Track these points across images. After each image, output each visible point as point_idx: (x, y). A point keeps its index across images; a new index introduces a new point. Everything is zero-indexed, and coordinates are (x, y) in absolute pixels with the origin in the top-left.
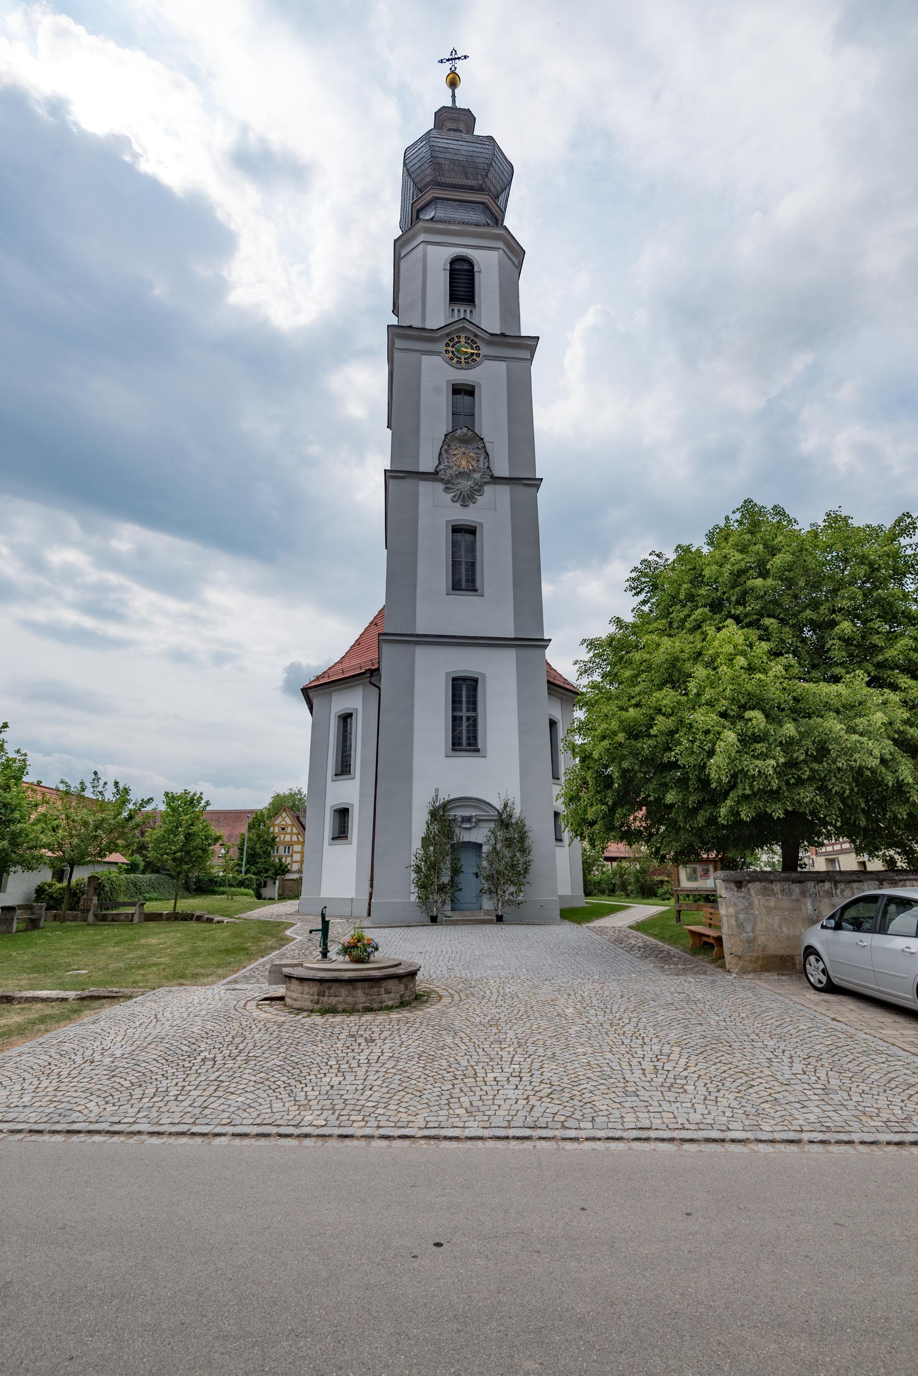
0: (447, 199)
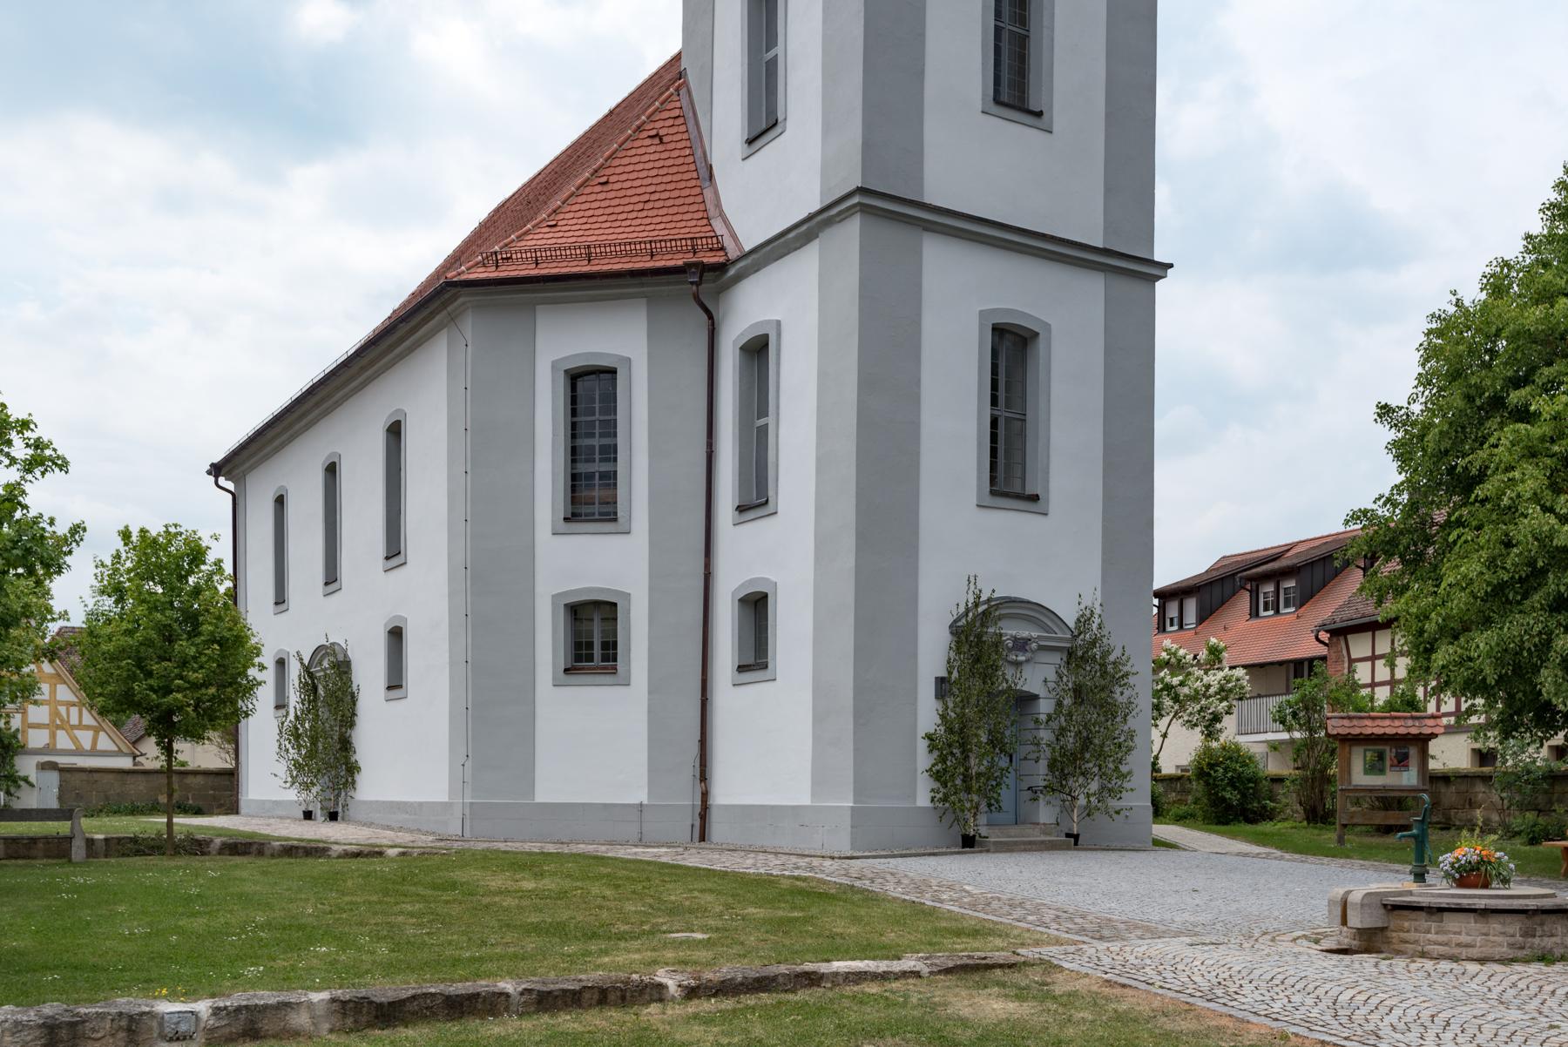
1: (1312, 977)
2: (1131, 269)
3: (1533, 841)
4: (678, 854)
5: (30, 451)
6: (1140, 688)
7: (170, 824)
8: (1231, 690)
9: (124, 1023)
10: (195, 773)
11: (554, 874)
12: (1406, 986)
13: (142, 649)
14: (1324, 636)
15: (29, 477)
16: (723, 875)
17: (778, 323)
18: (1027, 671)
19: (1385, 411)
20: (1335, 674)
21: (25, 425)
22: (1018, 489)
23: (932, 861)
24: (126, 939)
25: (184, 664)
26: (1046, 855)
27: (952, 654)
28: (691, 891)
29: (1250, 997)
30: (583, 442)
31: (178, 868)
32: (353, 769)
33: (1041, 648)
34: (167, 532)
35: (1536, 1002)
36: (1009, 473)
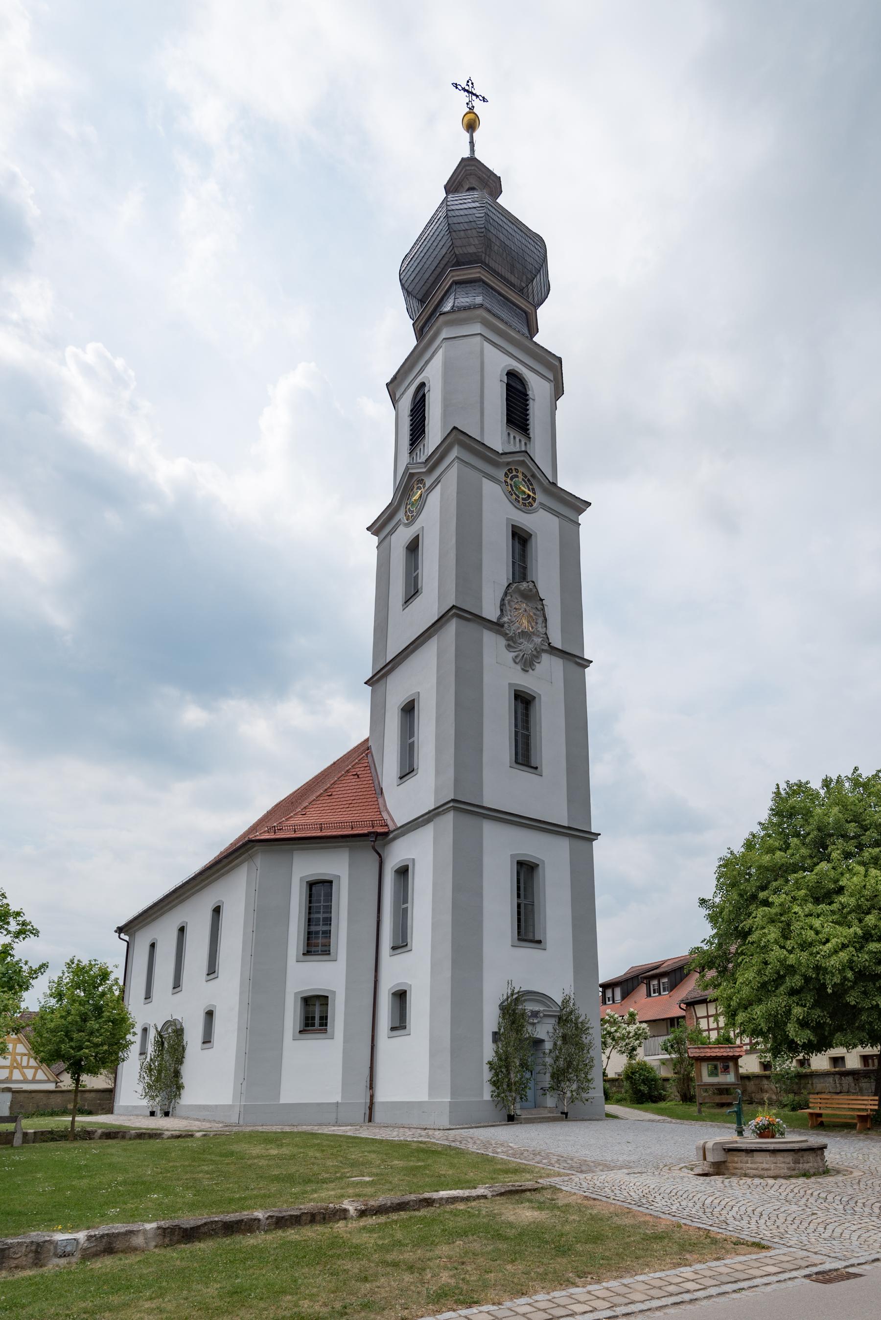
0: (492, 288)
1: (691, 1190)
2: (582, 836)
3: (794, 1109)
4: (356, 1130)
5: (19, 927)
6: (595, 1035)
7: (73, 1122)
8: (640, 1034)
9: (33, 1248)
10: (90, 1091)
11: (288, 1145)
12: (738, 1193)
13: (70, 1026)
14: (683, 1006)
15: (17, 940)
16: (381, 1142)
17: (414, 860)
18: (539, 1028)
19: (703, 902)
20: (690, 1025)
21: (18, 914)
22: (531, 937)
23: (492, 1130)
24: (41, 1195)
25: (91, 1033)
26: (551, 1124)
27: (501, 1020)
28: (363, 1152)
29: (660, 1204)
30: (314, 916)
31: (75, 1148)
32: (180, 1087)
33: (545, 1016)
34: (90, 964)
35: (804, 1200)
36: (527, 930)
